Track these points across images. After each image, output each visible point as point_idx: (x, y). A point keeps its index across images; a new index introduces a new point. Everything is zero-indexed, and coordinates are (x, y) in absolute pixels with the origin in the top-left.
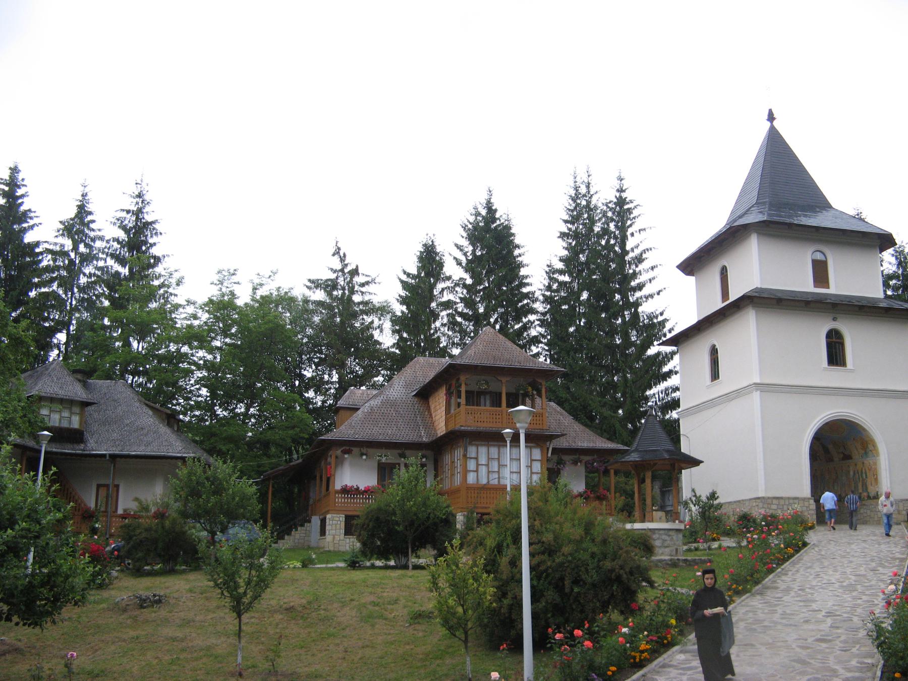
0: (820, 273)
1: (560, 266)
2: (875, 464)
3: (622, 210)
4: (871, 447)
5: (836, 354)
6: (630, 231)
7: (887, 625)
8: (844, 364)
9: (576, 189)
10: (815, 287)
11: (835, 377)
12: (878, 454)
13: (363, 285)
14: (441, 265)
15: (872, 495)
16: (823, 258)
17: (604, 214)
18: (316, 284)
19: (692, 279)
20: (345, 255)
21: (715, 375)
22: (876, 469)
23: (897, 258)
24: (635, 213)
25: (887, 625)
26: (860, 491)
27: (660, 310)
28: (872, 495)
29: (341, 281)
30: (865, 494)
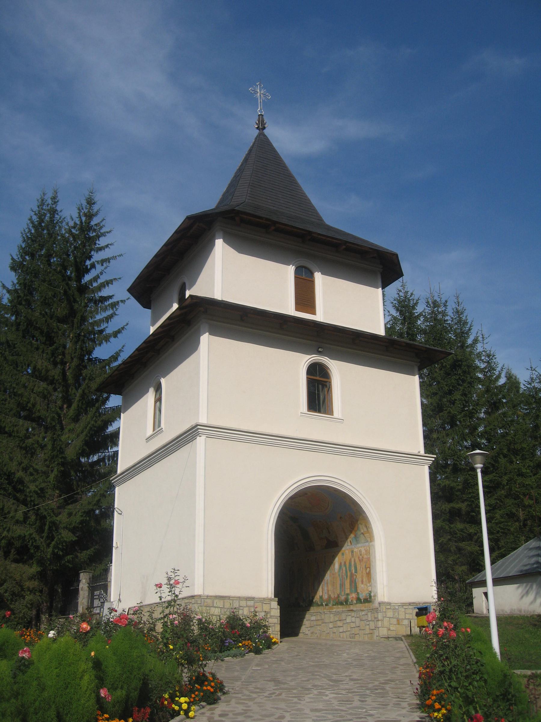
0: (305, 296)
2: (368, 552)
3: (87, 235)
4: (362, 529)
10: (297, 309)
11: (316, 427)
15: (362, 596)
19: (149, 311)
22: (369, 559)
24: (102, 242)
26: (348, 591)
28: (362, 596)
30: (354, 595)
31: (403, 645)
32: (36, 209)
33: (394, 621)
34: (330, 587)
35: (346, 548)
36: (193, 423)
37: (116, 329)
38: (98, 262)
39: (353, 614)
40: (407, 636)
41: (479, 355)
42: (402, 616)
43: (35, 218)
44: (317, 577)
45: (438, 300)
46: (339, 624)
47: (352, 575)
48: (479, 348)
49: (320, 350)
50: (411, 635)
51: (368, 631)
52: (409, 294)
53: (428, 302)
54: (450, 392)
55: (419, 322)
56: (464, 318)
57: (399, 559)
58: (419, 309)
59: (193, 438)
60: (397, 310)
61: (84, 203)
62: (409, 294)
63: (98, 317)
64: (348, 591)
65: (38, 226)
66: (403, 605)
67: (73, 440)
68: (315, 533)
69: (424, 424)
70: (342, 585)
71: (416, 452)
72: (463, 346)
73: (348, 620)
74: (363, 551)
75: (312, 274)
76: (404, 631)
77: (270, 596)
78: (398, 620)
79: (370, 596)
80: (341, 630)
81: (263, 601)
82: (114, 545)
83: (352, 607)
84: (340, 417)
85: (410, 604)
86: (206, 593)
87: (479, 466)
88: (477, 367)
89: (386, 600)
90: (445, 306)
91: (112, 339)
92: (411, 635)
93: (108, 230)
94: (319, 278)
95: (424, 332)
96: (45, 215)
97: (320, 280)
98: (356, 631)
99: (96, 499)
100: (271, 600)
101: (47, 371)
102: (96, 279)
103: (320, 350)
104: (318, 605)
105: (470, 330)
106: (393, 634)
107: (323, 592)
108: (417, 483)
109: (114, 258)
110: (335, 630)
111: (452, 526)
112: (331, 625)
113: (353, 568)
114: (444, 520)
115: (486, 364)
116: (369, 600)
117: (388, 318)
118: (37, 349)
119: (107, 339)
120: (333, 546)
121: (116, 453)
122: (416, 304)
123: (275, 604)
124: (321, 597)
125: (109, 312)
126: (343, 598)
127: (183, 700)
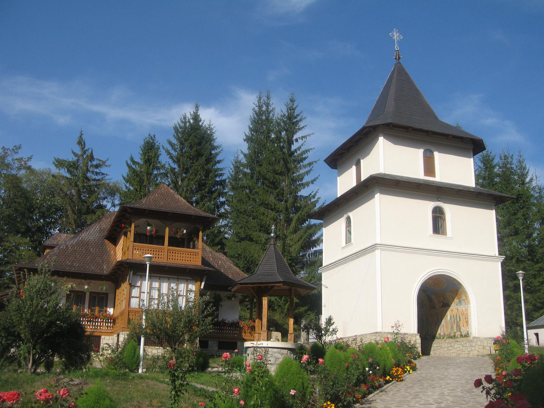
0: (429, 169)
1: (244, 161)
2: (467, 310)
4: (463, 297)
5: (438, 223)
6: (295, 137)
7: (251, 126)
8: (444, 233)
9: (260, 107)
12: (468, 303)
13: (97, 166)
14: (157, 156)
15: (463, 334)
17: (279, 124)
18: (59, 163)
20: (84, 144)
21: (348, 240)
22: (467, 314)
23: (484, 164)
24: (301, 124)
25: (251, 126)
26: (455, 331)
27: (313, 194)
28: (463, 334)
29: (81, 163)
30: (459, 333)
31: (487, 358)
32: (257, 103)
33: (481, 347)
34: (445, 329)
35: (453, 306)
36: (374, 243)
37: (313, 179)
38: (299, 138)
39: (458, 343)
40: (488, 355)
41: (534, 188)
42: (485, 344)
43: (257, 109)
44: (438, 323)
45: (507, 154)
46: (450, 348)
47: (457, 322)
48: (534, 184)
50: (491, 354)
51: (467, 352)
52: (489, 152)
53: (501, 157)
54: (515, 214)
55: (495, 170)
56: (524, 165)
57: (483, 312)
58: (496, 161)
59: (374, 251)
60: (482, 162)
61: (289, 102)
62: (489, 152)
63: (302, 171)
64: (455, 331)
65: (259, 114)
66: (486, 339)
67: (294, 244)
68: (437, 299)
69: (498, 232)
70: (452, 328)
71: (493, 255)
72: (523, 183)
73: (456, 346)
74: (464, 309)
75: (433, 153)
76: (487, 352)
77: (412, 332)
78: (483, 347)
79: (468, 334)
80: (451, 352)
81: (412, 335)
82: (323, 304)
83: (457, 339)
84: (451, 236)
85: (490, 338)
86: (383, 331)
87: (521, 278)
88: (532, 196)
89: (477, 336)
90: (512, 158)
91: (311, 185)
92: (491, 354)
94: (437, 155)
95: (499, 175)
96: (262, 107)
97: (437, 155)
98: (460, 352)
99: (309, 279)
100: (416, 335)
101: (275, 205)
102: (299, 148)
104: (438, 338)
105: (527, 173)
106: (481, 354)
107: (441, 331)
108: (495, 270)
109: (309, 135)
110: (448, 352)
111: (516, 294)
112: (446, 349)
113: (458, 319)
114: (511, 291)
115: (538, 194)
116: (467, 335)
117: (477, 168)
118: (267, 191)
119: (307, 184)
120: (446, 305)
121: (321, 252)
122: (493, 159)
123: (418, 337)
124: (440, 334)
125: (308, 169)
126: (452, 334)
127: (408, 367)
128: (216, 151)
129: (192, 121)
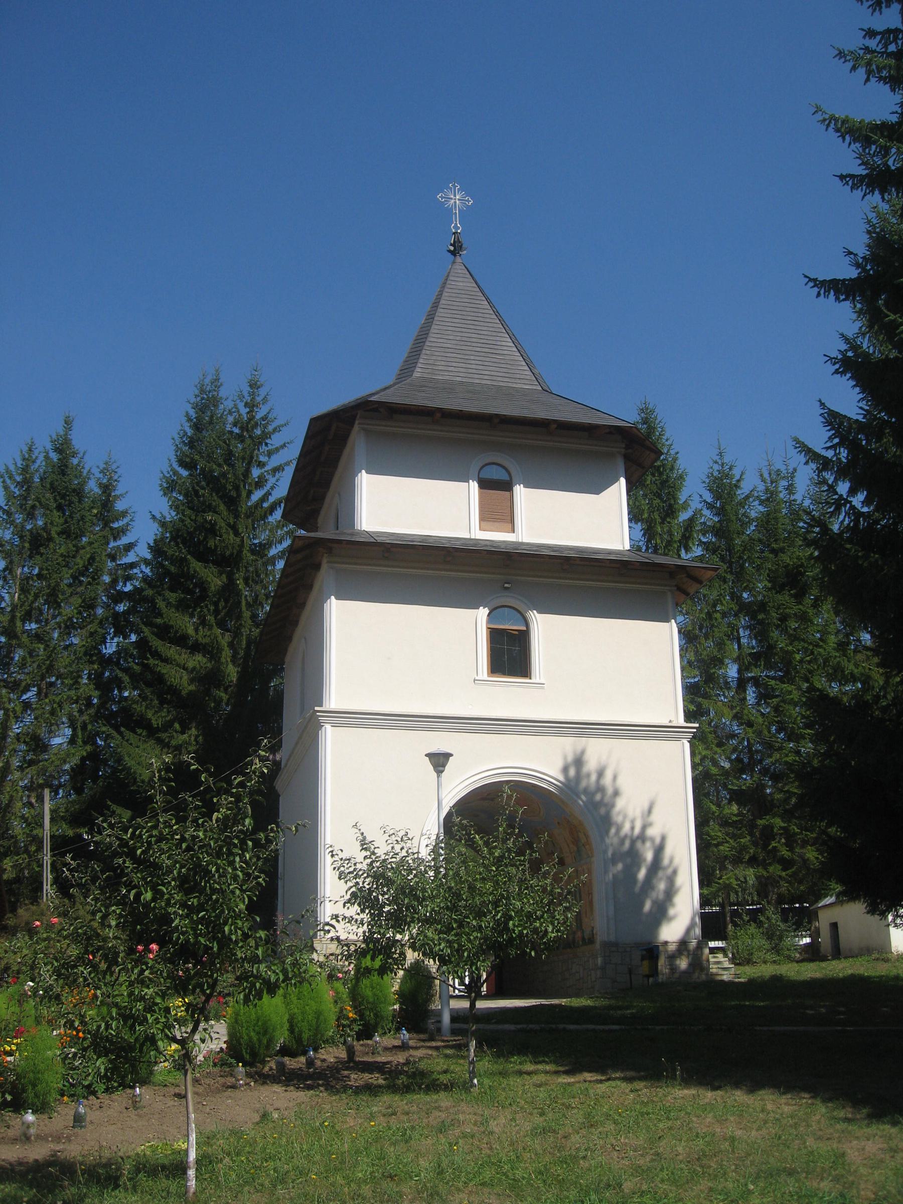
5: (510, 655)
11: (507, 698)
16: (504, 476)
37: (646, 806)
43: (192, 413)
45: (783, 468)
49: (506, 585)
93: (282, 423)
103: (506, 585)
128: (121, 523)
129: (54, 456)
